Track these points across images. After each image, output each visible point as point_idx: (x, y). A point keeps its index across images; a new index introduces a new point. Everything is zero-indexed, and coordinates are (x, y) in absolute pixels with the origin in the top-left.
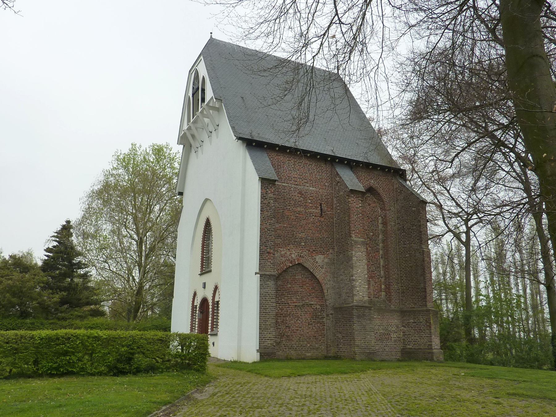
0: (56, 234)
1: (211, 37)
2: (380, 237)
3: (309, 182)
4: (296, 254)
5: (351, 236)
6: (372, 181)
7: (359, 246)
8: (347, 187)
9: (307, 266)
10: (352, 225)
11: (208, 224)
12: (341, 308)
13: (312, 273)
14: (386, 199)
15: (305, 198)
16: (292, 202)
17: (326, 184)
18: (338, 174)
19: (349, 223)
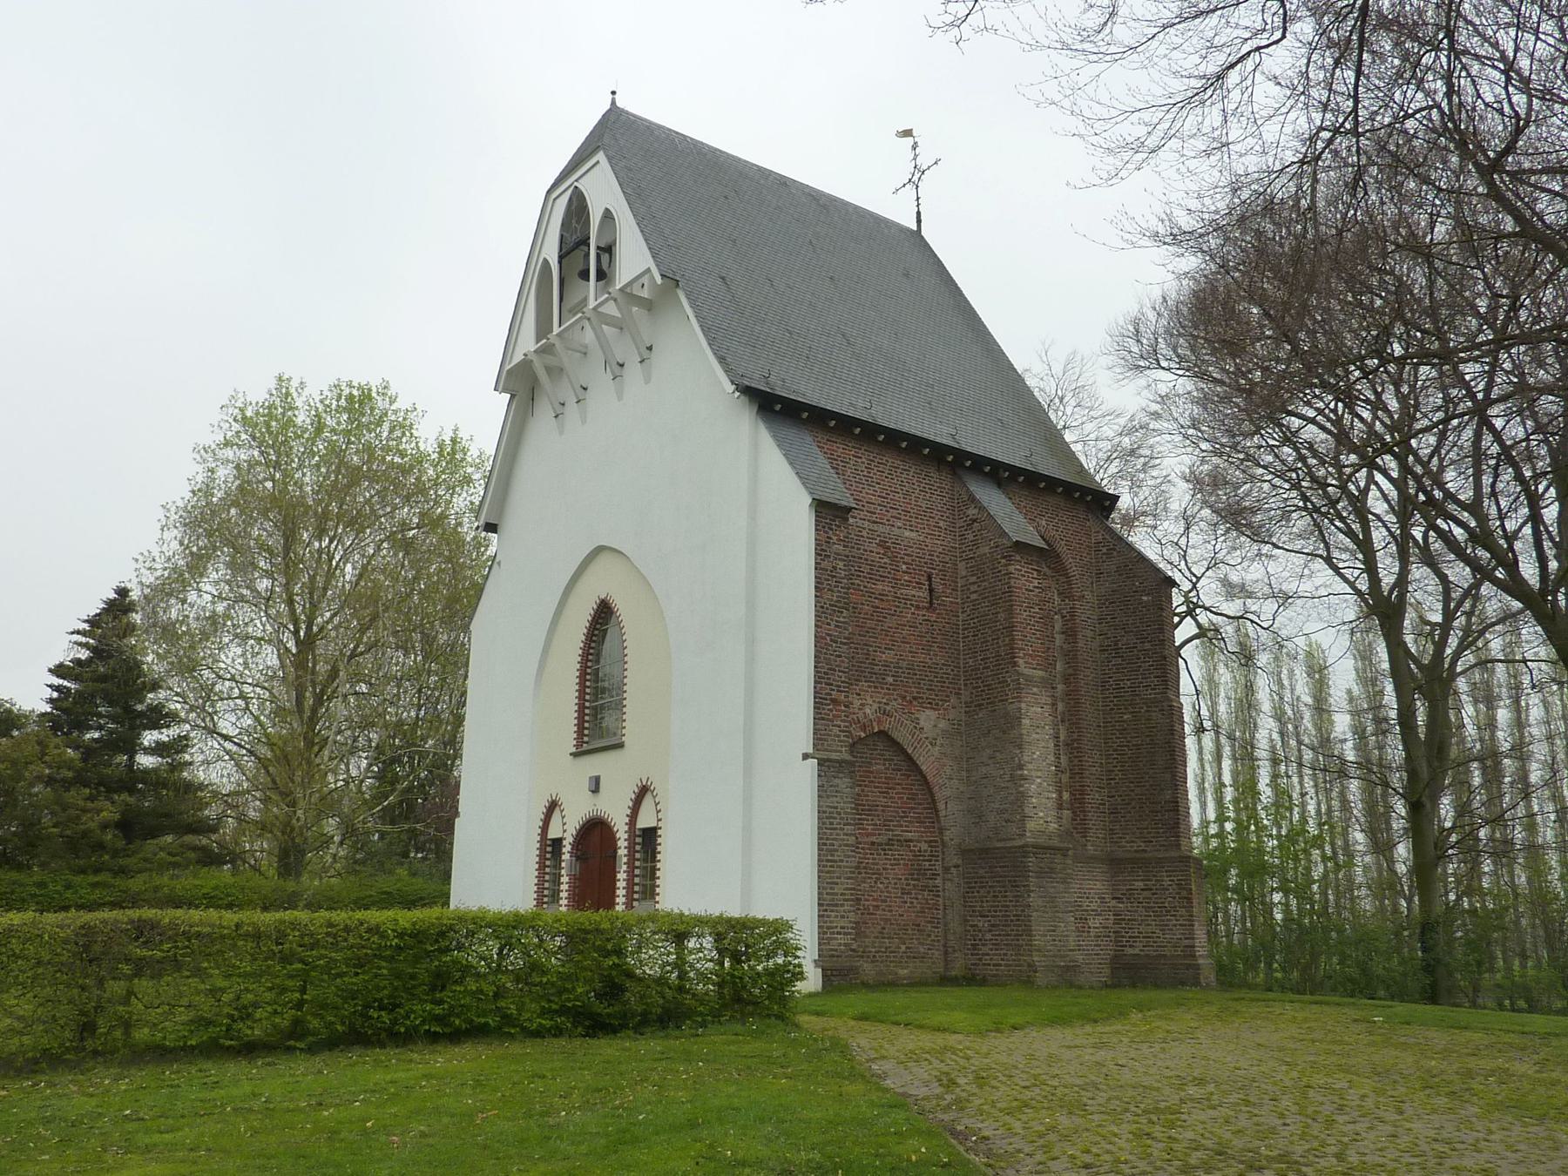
0: (86, 626)
1: (613, 102)
2: (1059, 666)
3: (910, 514)
4: (876, 706)
5: (1015, 664)
8: (1004, 534)
9: (900, 740)
10: (1018, 635)
11: (604, 614)
12: (986, 851)
13: (909, 758)
14: (1074, 571)
16: (866, 568)
17: (941, 524)
18: (972, 499)
19: (1011, 628)
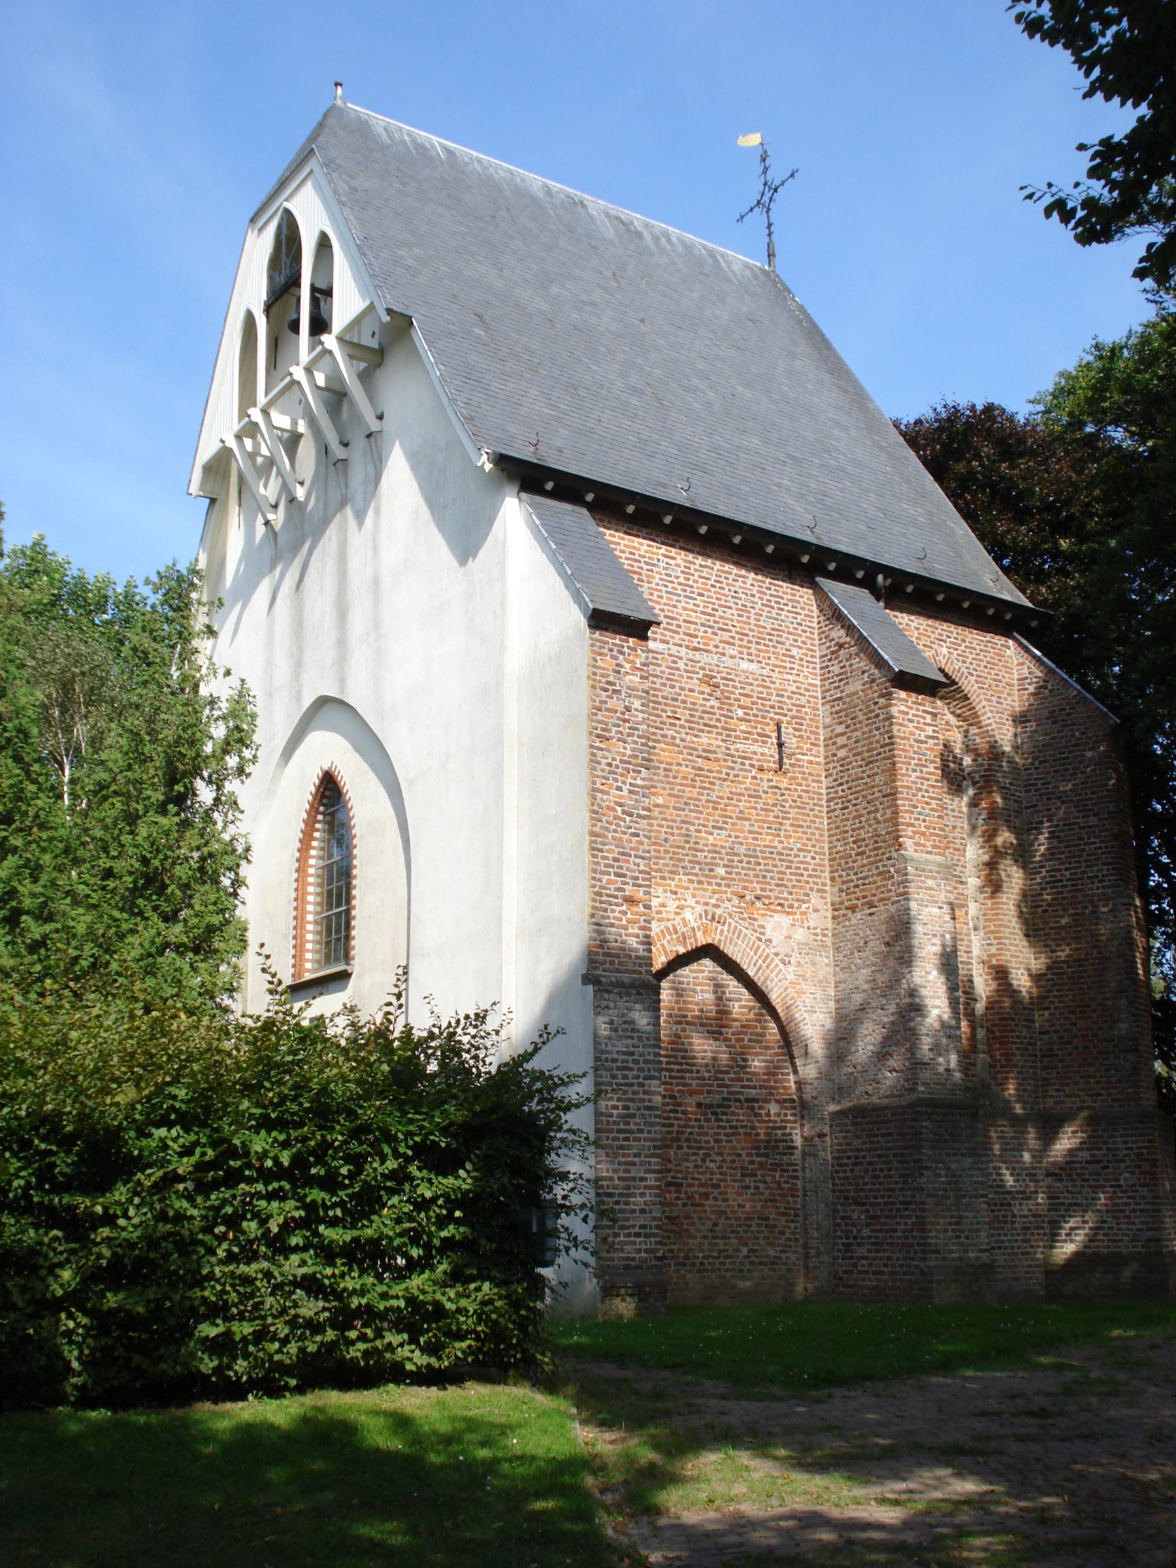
4: (700, 909)
6: (945, 651)
7: (930, 882)
9: (737, 957)
15: (724, 701)
16: (684, 714)
17: (794, 652)
19: (892, 795)
